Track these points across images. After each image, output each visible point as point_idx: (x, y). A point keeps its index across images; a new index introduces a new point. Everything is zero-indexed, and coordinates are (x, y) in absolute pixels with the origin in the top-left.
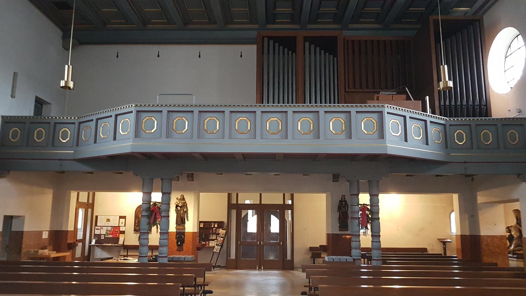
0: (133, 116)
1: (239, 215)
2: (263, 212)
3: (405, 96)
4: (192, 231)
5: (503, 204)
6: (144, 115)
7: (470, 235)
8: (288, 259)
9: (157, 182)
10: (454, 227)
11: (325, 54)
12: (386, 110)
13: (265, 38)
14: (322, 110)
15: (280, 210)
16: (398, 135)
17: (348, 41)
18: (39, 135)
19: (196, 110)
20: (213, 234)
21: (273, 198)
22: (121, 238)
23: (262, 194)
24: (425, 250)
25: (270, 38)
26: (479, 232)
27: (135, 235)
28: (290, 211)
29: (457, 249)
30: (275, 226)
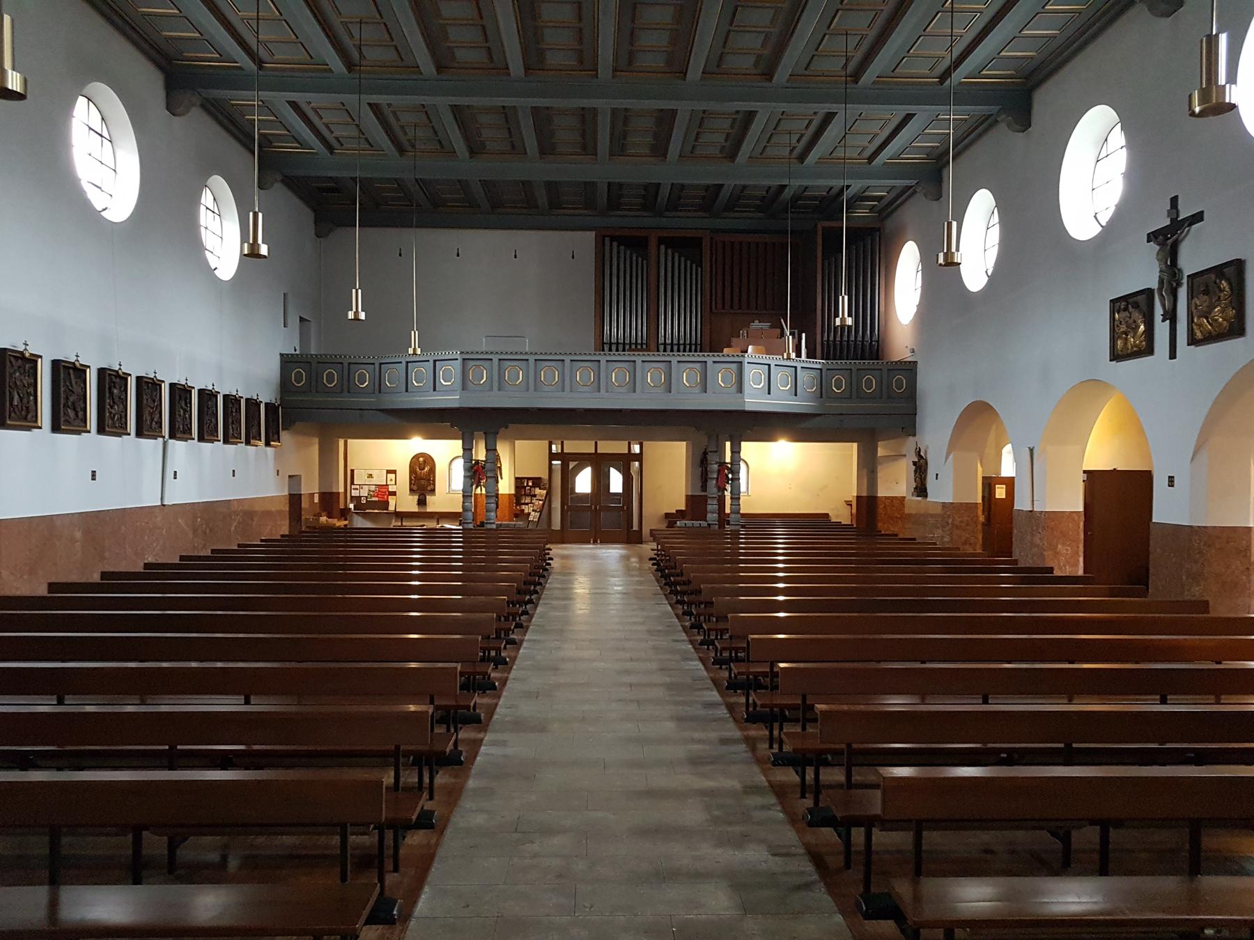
0: (459, 363)
1: (564, 467)
2: (601, 464)
3: (778, 331)
6: (472, 363)
14: (674, 360)
15: (624, 462)
18: (330, 380)
19: (532, 359)
20: (526, 495)
21: (619, 447)
22: (392, 501)
28: (637, 464)
30: (616, 482)
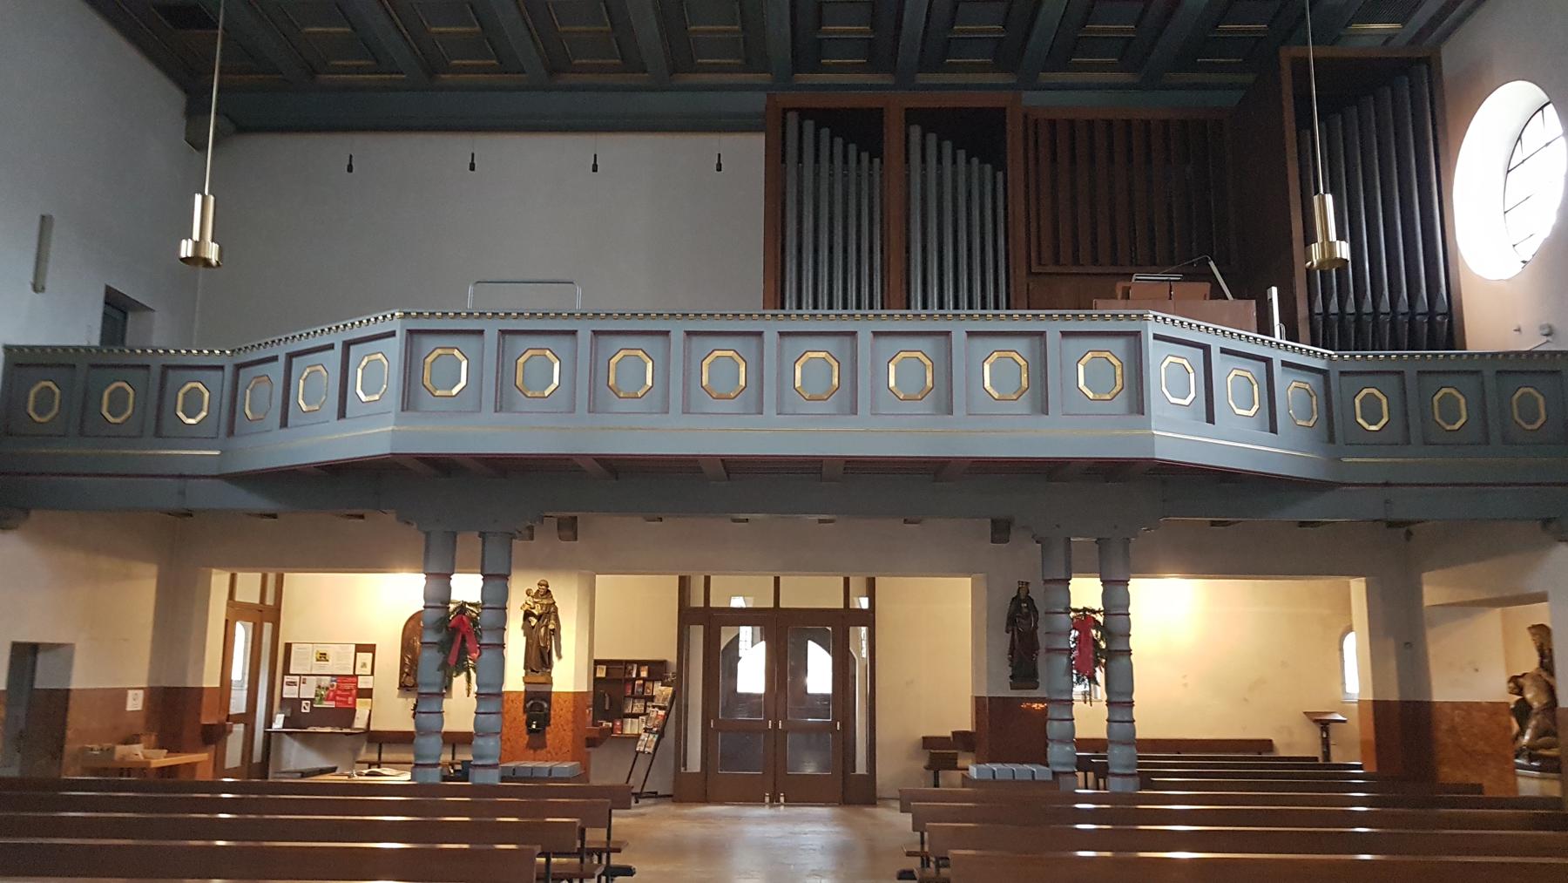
0: (395, 345)
1: (711, 641)
2: (785, 631)
3: (1206, 287)
4: (571, 689)
5: (1498, 610)
6: (428, 343)
7: (1401, 702)
8: (858, 772)
9: (469, 543)
10: (1354, 677)
11: (968, 162)
12: (1152, 328)
13: (789, 115)
14: (959, 330)
15: (835, 627)
16: (1187, 402)
17: (1036, 122)
18: (118, 404)
19: (584, 329)
20: (634, 697)
21: (813, 591)
22: (362, 709)
23: (782, 579)
24: (1267, 745)
25: (804, 113)
26: (1429, 691)
27: (402, 700)
28: (864, 630)
29: (1364, 743)
30: (819, 673)
